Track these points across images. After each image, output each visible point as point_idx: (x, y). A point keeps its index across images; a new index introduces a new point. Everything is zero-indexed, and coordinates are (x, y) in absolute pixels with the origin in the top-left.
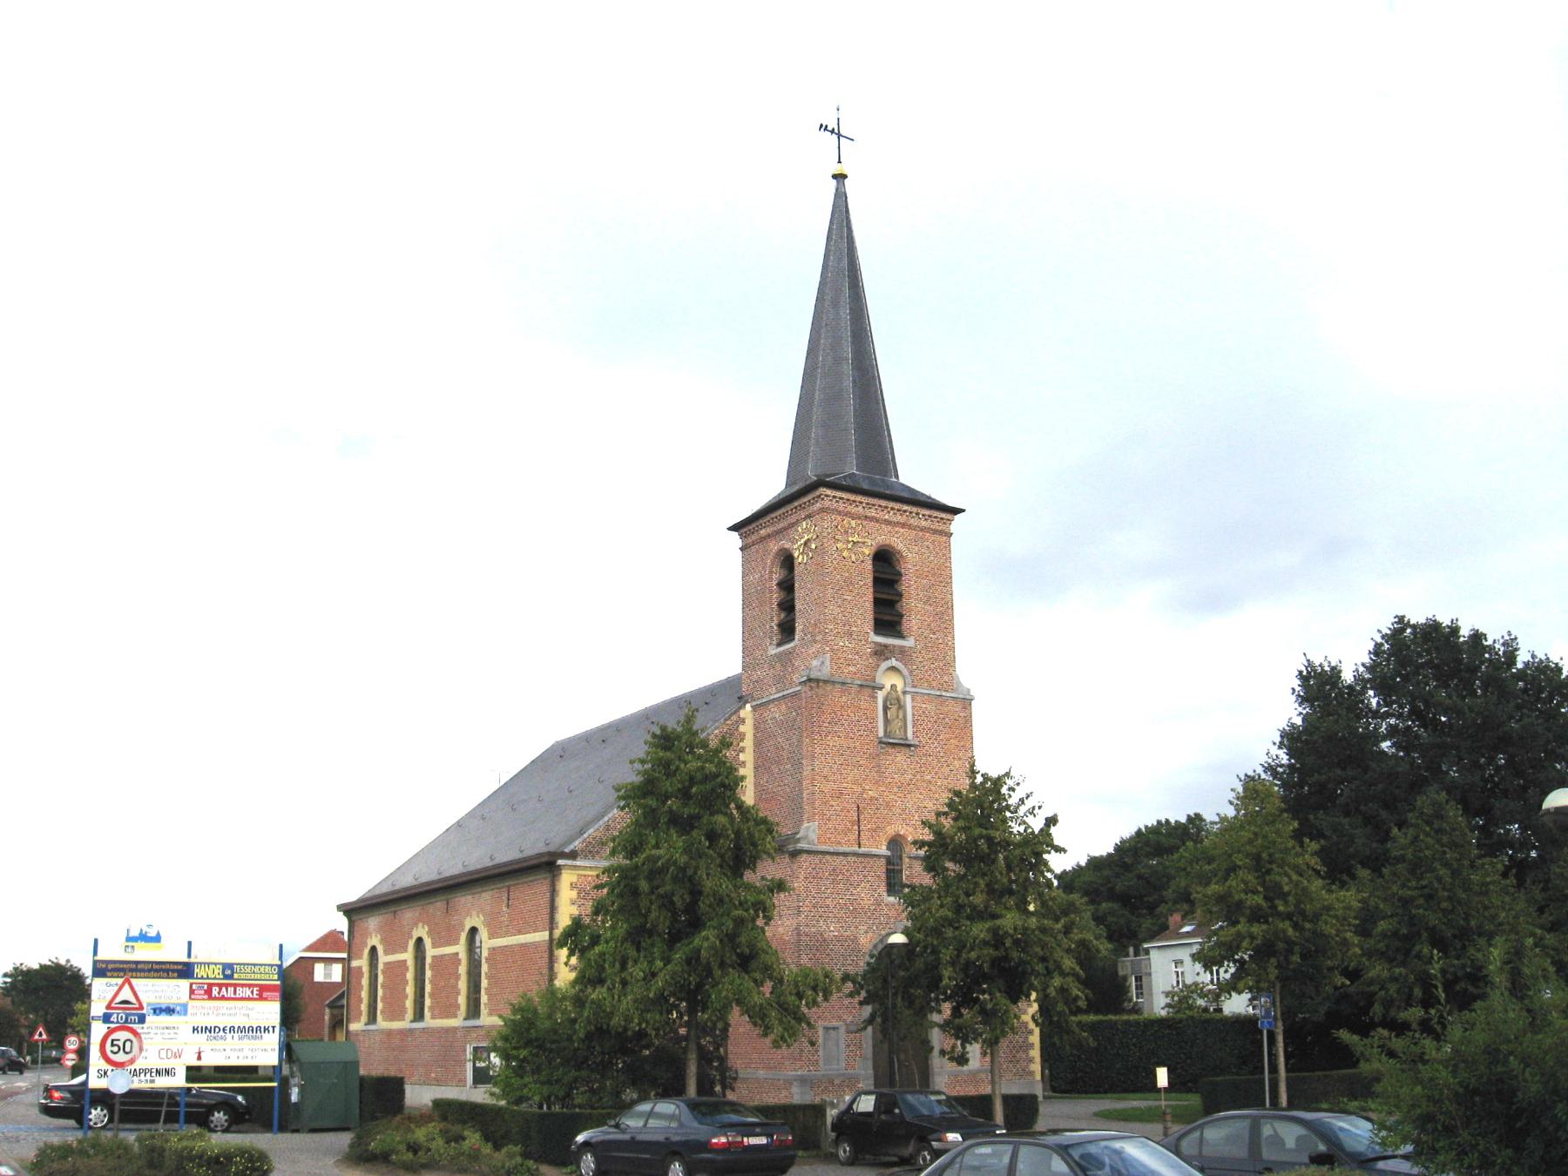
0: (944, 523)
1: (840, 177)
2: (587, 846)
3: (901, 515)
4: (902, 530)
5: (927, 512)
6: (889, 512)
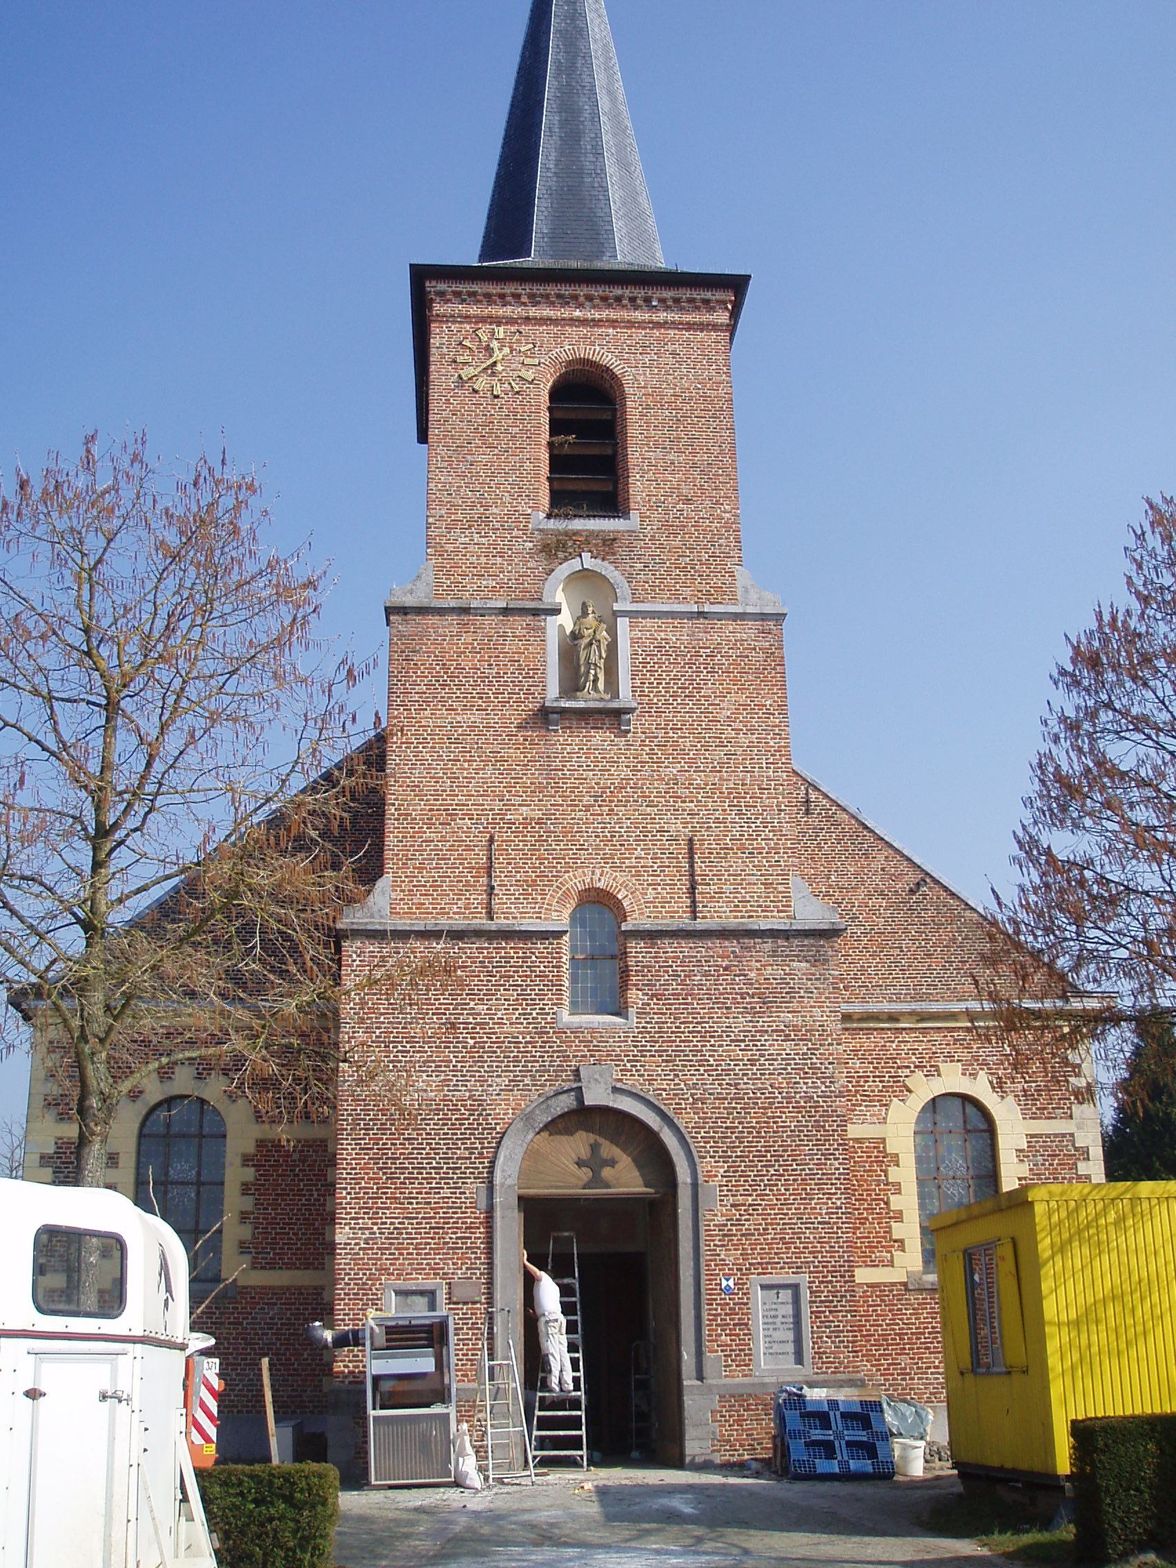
5: (668, 294)
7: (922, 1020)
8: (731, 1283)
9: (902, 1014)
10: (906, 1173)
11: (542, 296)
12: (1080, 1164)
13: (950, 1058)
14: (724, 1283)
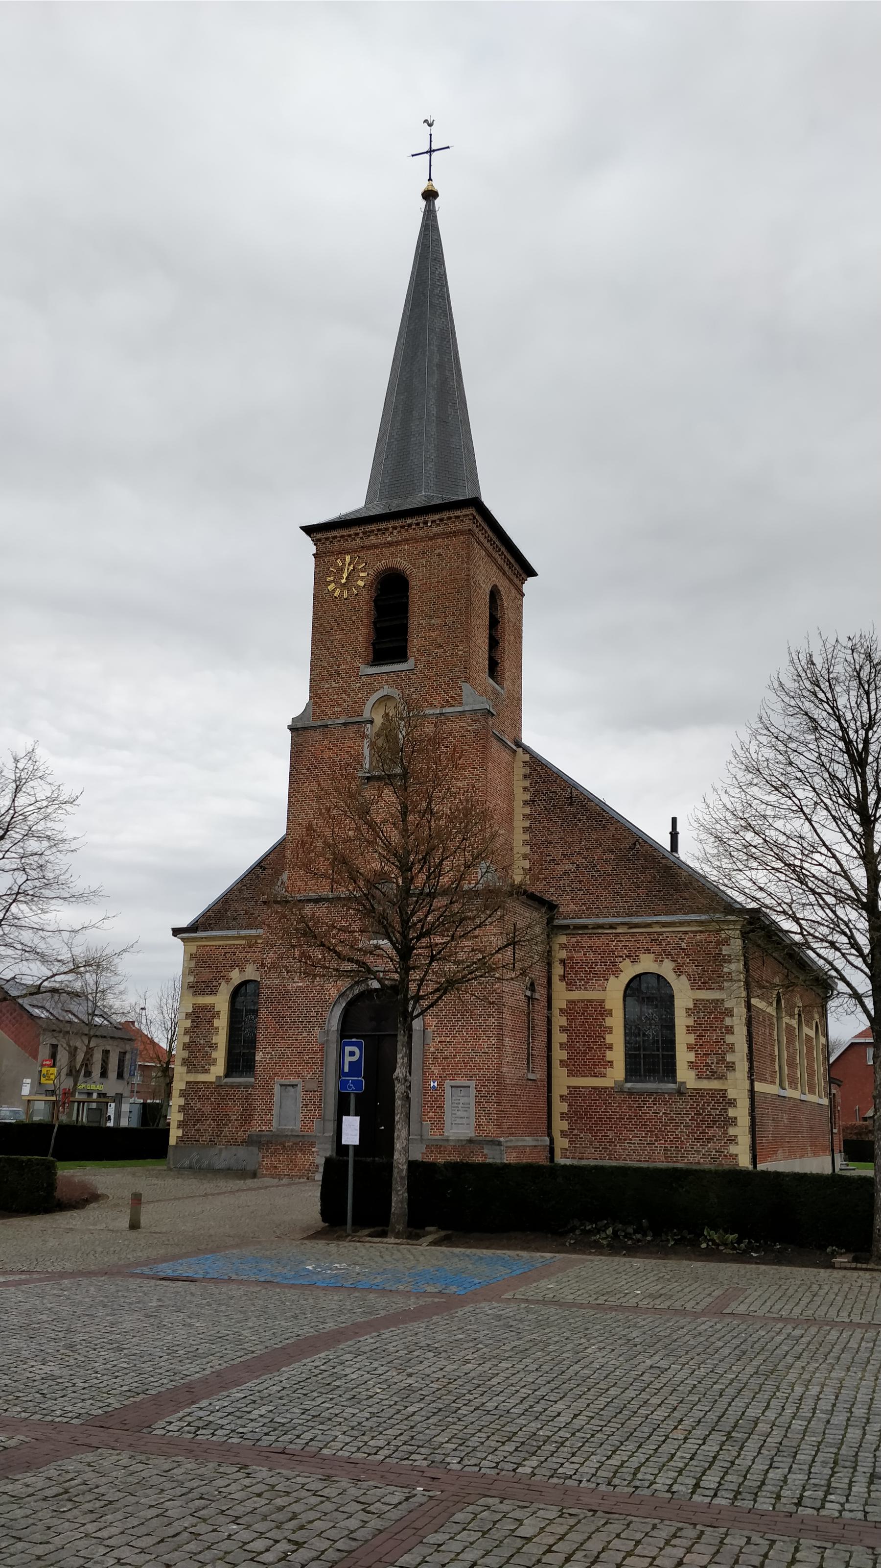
0: (446, 524)
1: (430, 195)
2: (207, 919)
3: (407, 530)
4: (406, 547)
5: (436, 517)
6: (392, 533)
7: (631, 928)
8: (436, 1084)
9: (618, 924)
10: (616, 1022)
11: (370, 532)
12: (727, 1018)
13: (648, 951)
14: (432, 1084)
